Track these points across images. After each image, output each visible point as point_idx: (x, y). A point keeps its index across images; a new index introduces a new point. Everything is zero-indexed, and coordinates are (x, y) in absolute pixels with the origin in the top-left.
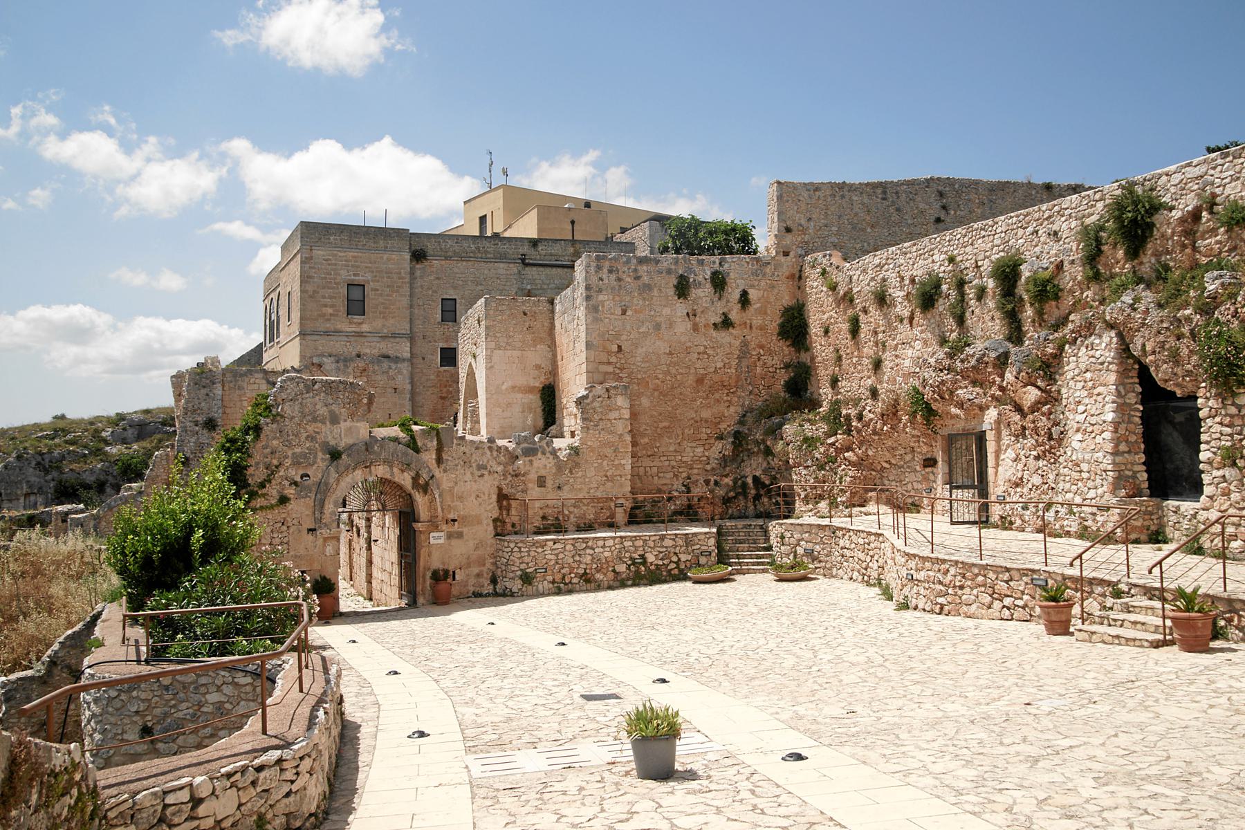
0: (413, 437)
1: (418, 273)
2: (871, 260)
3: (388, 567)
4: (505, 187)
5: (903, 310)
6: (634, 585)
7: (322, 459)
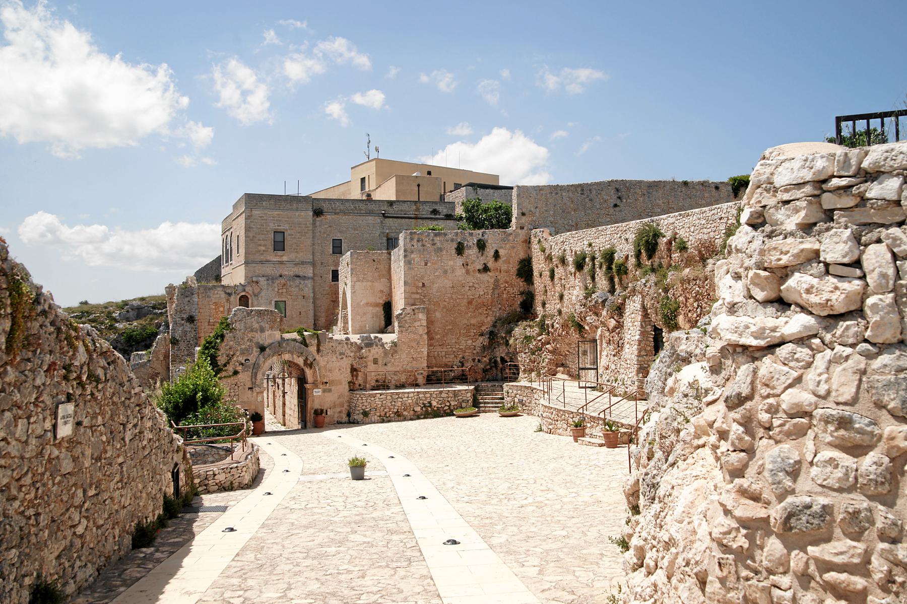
0: (304, 339)
1: (318, 223)
2: (560, 238)
3: (293, 407)
4: (378, 160)
5: (571, 268)
6: (424, 418)
7: (256, 351)
